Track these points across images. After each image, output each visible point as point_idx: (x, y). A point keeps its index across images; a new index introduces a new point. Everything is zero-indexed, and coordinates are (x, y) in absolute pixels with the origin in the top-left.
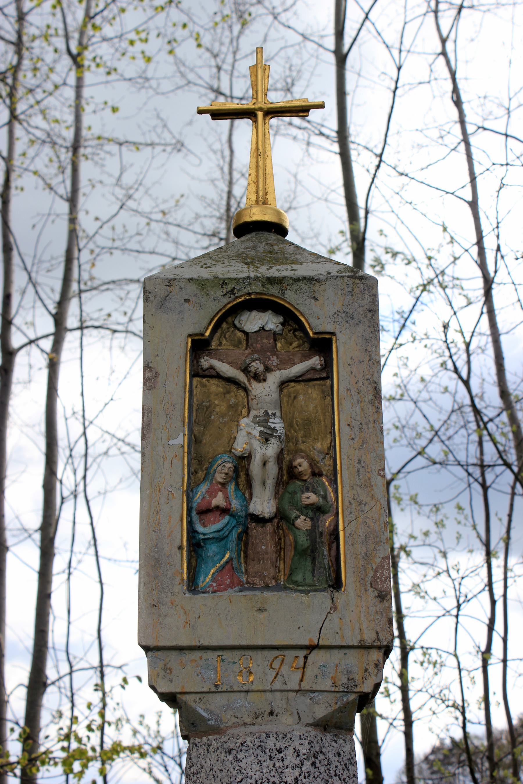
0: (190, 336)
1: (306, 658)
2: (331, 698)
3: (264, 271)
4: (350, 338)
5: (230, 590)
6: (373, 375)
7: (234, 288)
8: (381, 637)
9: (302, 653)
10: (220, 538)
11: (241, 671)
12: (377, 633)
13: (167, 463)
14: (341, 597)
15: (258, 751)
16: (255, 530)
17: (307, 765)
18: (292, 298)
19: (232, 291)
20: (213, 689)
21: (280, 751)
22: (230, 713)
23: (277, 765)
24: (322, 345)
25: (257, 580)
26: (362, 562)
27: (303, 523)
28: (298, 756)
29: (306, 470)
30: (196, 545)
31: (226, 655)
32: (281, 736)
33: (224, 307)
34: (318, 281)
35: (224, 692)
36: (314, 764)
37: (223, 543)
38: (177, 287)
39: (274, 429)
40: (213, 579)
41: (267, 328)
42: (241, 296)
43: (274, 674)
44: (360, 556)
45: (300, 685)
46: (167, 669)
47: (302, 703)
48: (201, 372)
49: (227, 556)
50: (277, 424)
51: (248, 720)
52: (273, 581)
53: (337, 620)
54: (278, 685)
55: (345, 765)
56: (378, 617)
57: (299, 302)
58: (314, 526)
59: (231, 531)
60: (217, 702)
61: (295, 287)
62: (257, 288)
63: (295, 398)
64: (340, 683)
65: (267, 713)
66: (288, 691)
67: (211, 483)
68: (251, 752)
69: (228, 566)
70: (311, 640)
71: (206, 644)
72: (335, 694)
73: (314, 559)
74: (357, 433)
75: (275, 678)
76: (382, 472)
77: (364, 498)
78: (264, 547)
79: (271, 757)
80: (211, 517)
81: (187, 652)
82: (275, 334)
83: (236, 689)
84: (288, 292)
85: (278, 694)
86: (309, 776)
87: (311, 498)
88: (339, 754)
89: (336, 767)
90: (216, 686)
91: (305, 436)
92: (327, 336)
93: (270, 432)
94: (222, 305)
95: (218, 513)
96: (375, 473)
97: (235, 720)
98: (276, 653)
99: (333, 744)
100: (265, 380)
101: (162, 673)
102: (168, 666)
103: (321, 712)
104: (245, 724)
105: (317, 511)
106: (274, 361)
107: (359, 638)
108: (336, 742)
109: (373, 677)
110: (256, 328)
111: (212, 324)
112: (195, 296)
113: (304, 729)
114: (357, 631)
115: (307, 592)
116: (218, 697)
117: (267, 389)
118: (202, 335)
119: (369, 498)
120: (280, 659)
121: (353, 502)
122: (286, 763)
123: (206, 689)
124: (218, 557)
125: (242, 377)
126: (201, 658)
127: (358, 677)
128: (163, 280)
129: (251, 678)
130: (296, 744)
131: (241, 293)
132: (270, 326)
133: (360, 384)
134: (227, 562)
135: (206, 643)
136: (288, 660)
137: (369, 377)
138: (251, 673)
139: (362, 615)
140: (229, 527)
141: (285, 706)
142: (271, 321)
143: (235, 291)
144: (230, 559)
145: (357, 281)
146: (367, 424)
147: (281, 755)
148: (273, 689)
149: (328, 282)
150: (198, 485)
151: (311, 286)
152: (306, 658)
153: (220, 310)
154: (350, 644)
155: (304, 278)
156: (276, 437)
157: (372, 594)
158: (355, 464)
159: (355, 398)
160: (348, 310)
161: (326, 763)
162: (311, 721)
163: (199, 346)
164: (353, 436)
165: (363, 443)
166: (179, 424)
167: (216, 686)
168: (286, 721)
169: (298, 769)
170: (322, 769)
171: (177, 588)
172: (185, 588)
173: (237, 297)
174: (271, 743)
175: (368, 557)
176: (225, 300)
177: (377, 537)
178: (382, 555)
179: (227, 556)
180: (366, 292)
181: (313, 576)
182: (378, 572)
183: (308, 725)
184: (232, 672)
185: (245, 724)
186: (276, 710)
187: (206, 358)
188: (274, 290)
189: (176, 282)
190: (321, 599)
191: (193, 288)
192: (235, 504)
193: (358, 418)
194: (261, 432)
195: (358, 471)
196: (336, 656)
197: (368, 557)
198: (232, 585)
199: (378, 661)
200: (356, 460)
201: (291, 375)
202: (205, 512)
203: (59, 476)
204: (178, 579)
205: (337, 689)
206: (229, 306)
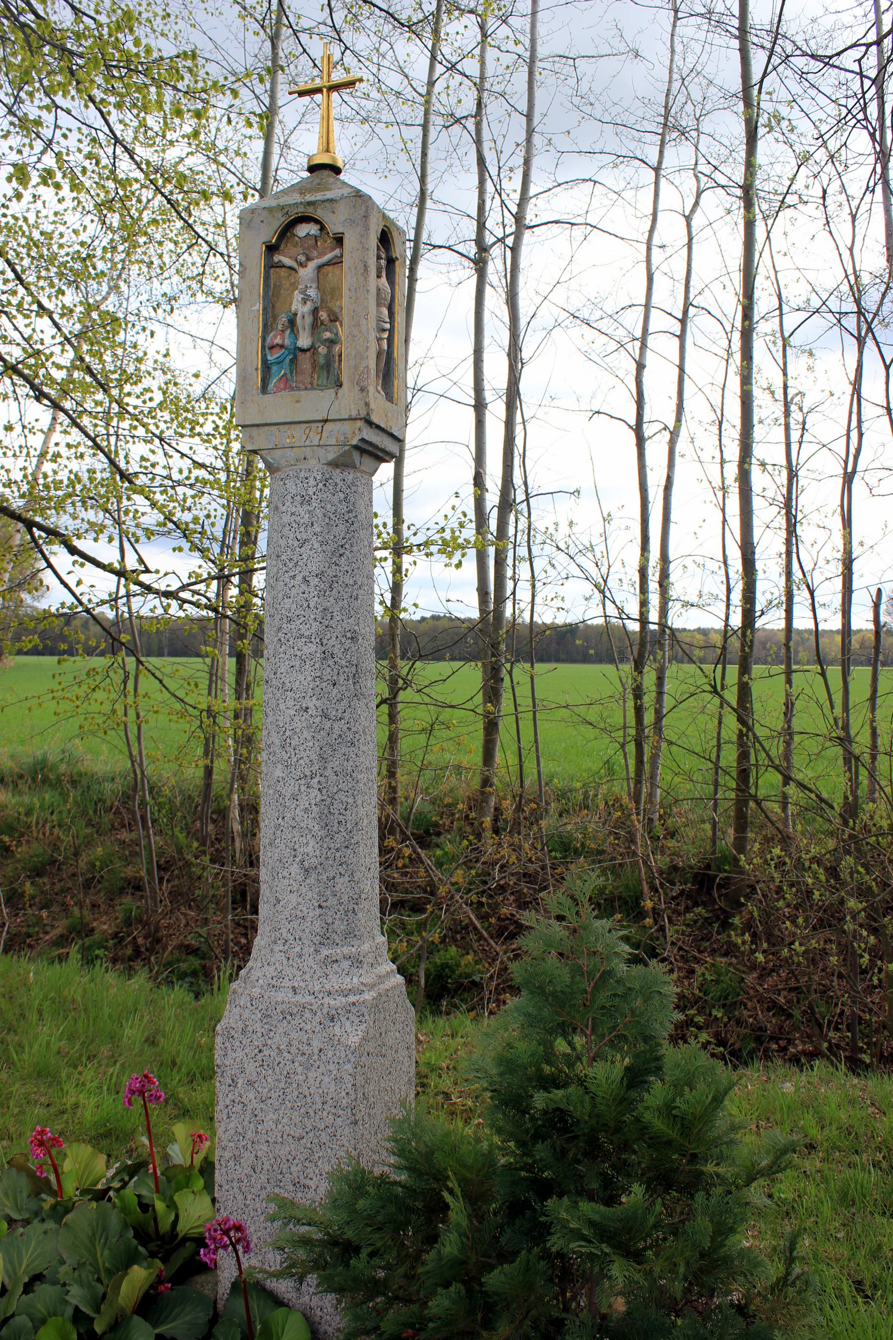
3: (309, 198)
10: (279, 362)
14: (341, 392)
16: (301, 357)
18: (320, 214)
24: (339, 240)
27: (322, 350)
30: (266, 367)
46: (251, 437)
47: (321, 452)
50: (312, 292)
58: (329, 352)
60: (278, 453)
62: (301, 209)
87: (328, 335)
103: (331, 457)
105: (332, 342)
106: (315, 253)
125: (295, 265)
132: (313, 232)
142: (313, 229)
157: (357, 388)
163: (271, 249)
168: (313, 462)
174: (302, 475)
175: (356, 367)
184: (285, 437)
190: (332, 392)
191: (265, 213)
192: (287, 342)
196: (338, 424)
197: (356, 367)
202: (272, 348)
203: (740, 308)
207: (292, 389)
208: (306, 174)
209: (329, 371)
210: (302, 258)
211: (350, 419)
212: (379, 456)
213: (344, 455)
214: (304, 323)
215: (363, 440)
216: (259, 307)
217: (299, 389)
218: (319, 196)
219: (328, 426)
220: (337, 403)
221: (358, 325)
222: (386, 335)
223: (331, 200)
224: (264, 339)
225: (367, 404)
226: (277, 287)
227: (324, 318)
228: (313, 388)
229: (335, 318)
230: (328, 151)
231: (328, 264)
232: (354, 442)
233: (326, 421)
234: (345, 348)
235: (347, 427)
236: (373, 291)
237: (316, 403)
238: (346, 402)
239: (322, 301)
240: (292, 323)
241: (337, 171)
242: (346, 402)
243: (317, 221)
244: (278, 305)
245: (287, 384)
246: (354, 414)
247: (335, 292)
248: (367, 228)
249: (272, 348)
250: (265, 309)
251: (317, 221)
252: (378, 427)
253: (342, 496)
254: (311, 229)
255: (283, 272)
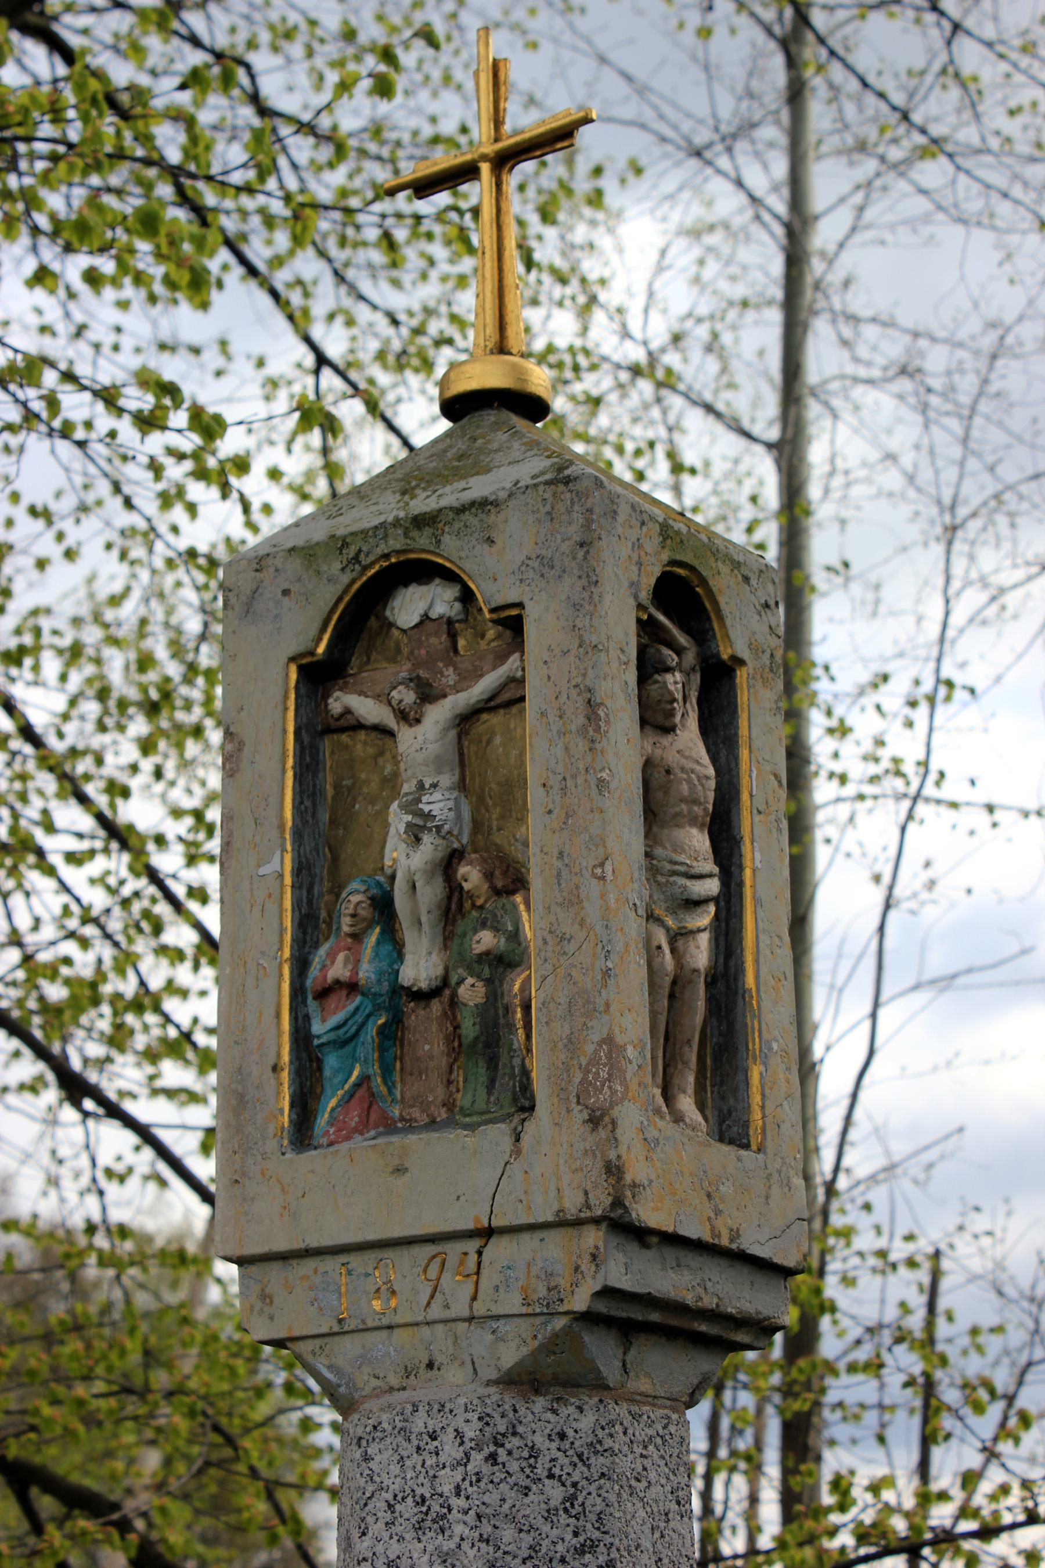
0: (292, 659)
1: (480, 1253)
2: (524, 1327)
3: (423, 503)
4: (547, 609)
5: (358, 1138)
6: (584, 675)
7: (360, 551)
8: (592, 1201)
9: (472, 1246)
10: (345, 1040)
11: (378, 1290)
12: (586, 1193)
13: (257, 910)
15: (400, 1439)
17: (477, 1458)
19: (356, 559)
20: (336, 1328)
21: (433, 1437)
22: (367, 1370)
23: (428, 1463)
24: (512, 624)
25: (416, 1113)
26: (562, 1057)
27: (471, 992)
28: (462, 1443)
29: (476, 887)
31: (355, 1260)
32: (436, 1407)
33: (345, 591)
34: (496, 504)
35: (353, 1331)
36: (492, 1458)
37: (348, 1049)
38: (272, 570)
39: (429, 816)
40: (331, 1124)
41: (434, 615)
42: (373, 563)
43: (429, 1291)
44: (560, 1045)
45: (471, 1307)
46: (266, 1298)
48: (333, 724)
49: (356, 1073)
50: (438, 804)
51: (394, 1381)
52: (443, 1110)
53: (520, 1177)
54: (436, 1312)
55: (580, 1456)
56: (589, 1161)
57: (463, 554)
59: (363, 1025)
60: (348, 1348)
61: (457, 525)
62: (396, 542)
63: (489, 742)
64: (535, 1297)
65: (423, 1366)
66: (454, 1320)
67: (338, 935)
68: (389, 1440)
69: (362, 1092)
70: (477, 1219)
71: (314, 1244)
72: (532, 1320)
73: (493, 1063)
74: (557, 798)
75: (432, 1297)
76: (599, 871)
77: (568, 927)
78: (427, 1047)
79: (418, 1448)
80: (332, 1001)
81: (294, 1262)
82: (450, 622)
83: (370, 1324)
84: (446, 539)
85: (440, 1327)
86: (479, 1480)
87: (486, 940)
88: (562, 1436)
89: (552, 1460)
90: (340, 1321)
91: (502, 817)
92: (514, 612)
93: (420, 822)
94: (340, 588)
95: (344, 993)
96: (587, 874)
97: (374, 1383)
98: (430, 1249)
99: (549, 1415)
100: (418, 721)
101: (258, 1305)
102: (267, 1291)
103: (510, 1356)
104: (391, 1389)
106: (450, 676)
107: (556, 1208)
108: (554, 1412)
109: (590, 1281)
110: (415, 619)
111: (330, 630)
112: (299, 580)
113: (482, 1391)
114: (553, 1193)
115: (472, 1127)
116: (347, 1340)
117: (420, 738)
118: (312, 653)
119: (577, 927)
120: (438, 1260)
121: (549, 938)
122: (442, 1458)
123: (325, 1330)
124: (340, 1077)
125: (390, 720)
126: (316, 1271)
127: (563, 1283)
128: (250, 561)
129: (393, 1303)
130: (459, 1422)
131: (371, 558)
132: (440, 609)
133: (563, 698)
134: (357, 1085)
135: (314, 1243)
136: (452, 1260)
137: (579, 680)
138: (394, 1292)
139: (562, 1161)
140: (359, 1018)
141: (451, 1351)
143: (362, 556)
144: (364, 1080)
145: (562, 488)
146: (574, 777)
147: (435, 1443)
148: (429, 1318)
149: (512, 503)
150: (316, 945)
151: (484, 516)
152: (480, 1253)
153: (340, 599)
154: (541, 1220)
155: (473, 503)
156: (430, 830)
157: (579, 1115)
158: (554, 861)
159: (554, 729)
160: (543, 552)
161: (526, 1454)
162: (494, 1375)
163: (318, 676)
164: (551, 806)
165: (567, 816)
166: (275, 833)
167: (340, 1321)
168: (455, 1375)
169: (461, 1469)
170: (514, 1466)
171: (271, 1145)
172: (286, 1142)
173: (365, 568)
174: (419, 1423)
175: (572, 1044)
176: (345, 579)
177: (588, 1002)
178: (596, 1038)
179: (356, 1073)
180: (576, 508)
181: (489, 1093)
182: (589, 1072)
183: (489, 1383)
185: (391, 1389)
186: (439, 1359)
187: (337, 694)
188: (423, 539)
189: (270, 561)
190: (498, 1134)
191: (295, 565)
192: (366, 972)
193: (560, 769)
194: (409, 825)
195: (559, 875)
196: (529, 1241)
197: (572, 1044)
198: (361, 1129)
199: (596, 1247)
200: (556, 854)
201: (473, 700)
202: (324, 993)
204: (271, 1129)
205: (530, 1310)
206: (356, 586)
207: (389, 1127)
208: (444, 425)
209: (489, 1063)
210: (406, 696)
211: (563, 1223)
212: (711, 1337)
213: (552, 1345)
214: (418, 903)
215: (607, 1292)
216: (283, 863)
217: (410, 1126)
218: (450, 496)
219: (498, 1250)
220: (516, 1168)
221: (574, 901)
222: (704, 918)
223: (483, 505)
224: (301, 964)
225: (614, 1170)
226: (345, 794)
227: (483, 877)
228: (451, 1123)
229: (511, 880)
230: (502, 348)
231: (489, 705)
232: (580, 1302)
233: (488, 1233)
234: (536, 983)
235: (554, 1251)
236: (627, 780)
237: (453, 1174)
238: (546, 1165)
239: (477, 826)
240: (383, 906)
241: (533, 408)
242: (546, 1165)
243: (449, 576)
244: (348, 851)
245: (372, 1115)
246: (572, 1203)
247: (510, 798)
248: (591, 581)
249: (324, 993)
250: (301, 869)
251: (449, 576)
252: (673, 1240)
253: (556, 1493)
254: (434, 600)
255: (361, 745)
